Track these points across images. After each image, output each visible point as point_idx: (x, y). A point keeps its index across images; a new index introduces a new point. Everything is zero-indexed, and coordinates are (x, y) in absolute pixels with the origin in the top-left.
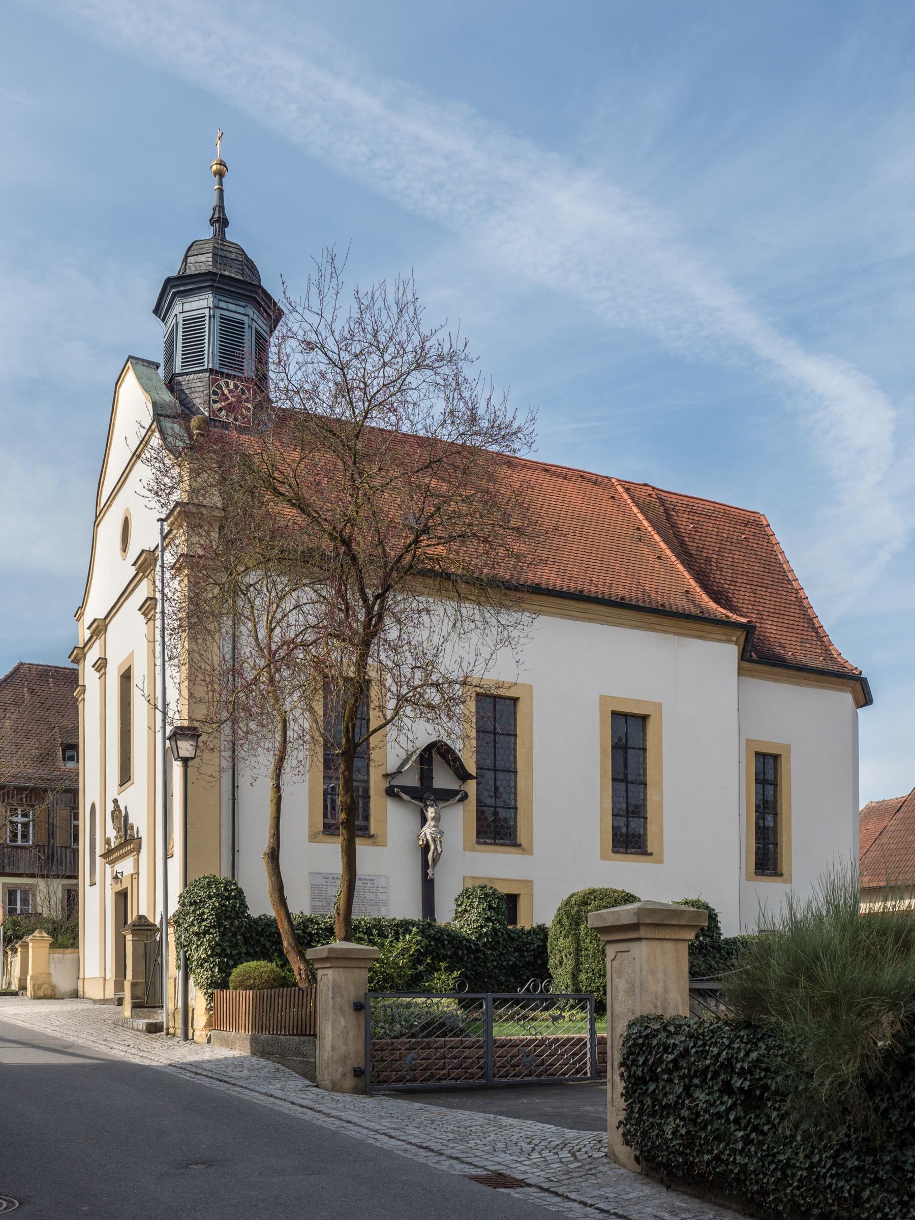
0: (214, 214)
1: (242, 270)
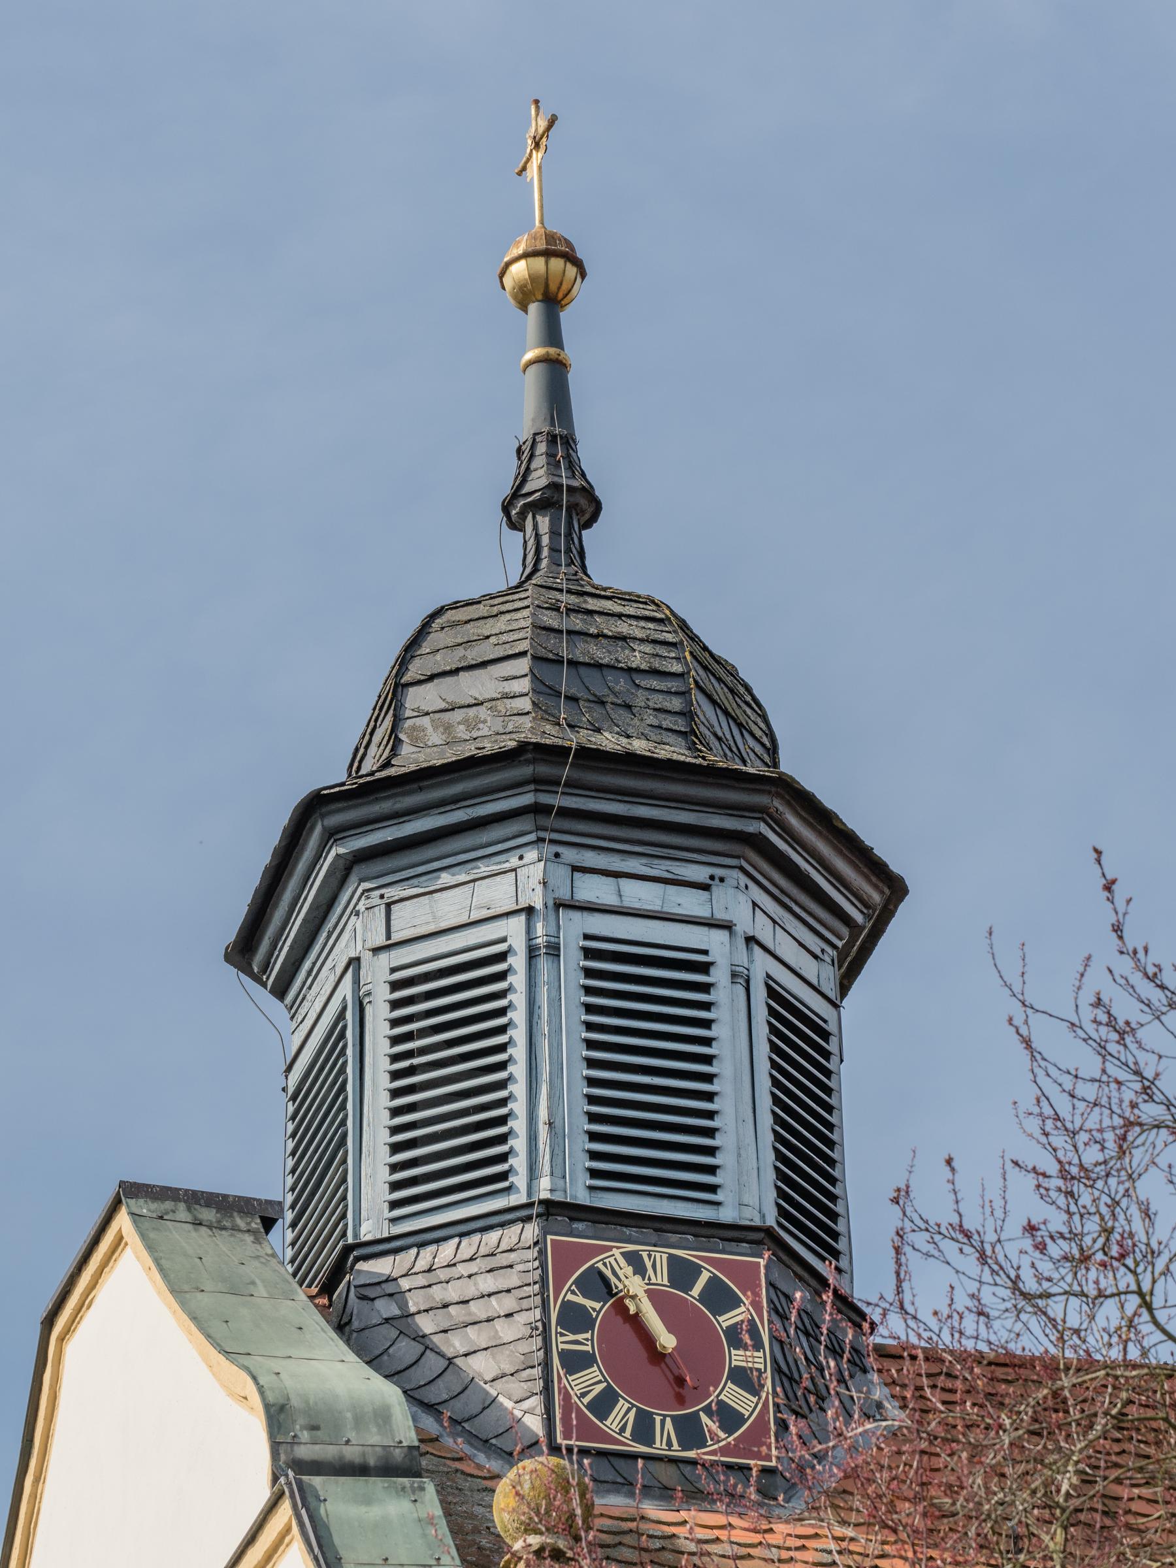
0: (524, 478)
1: (688, 714)
